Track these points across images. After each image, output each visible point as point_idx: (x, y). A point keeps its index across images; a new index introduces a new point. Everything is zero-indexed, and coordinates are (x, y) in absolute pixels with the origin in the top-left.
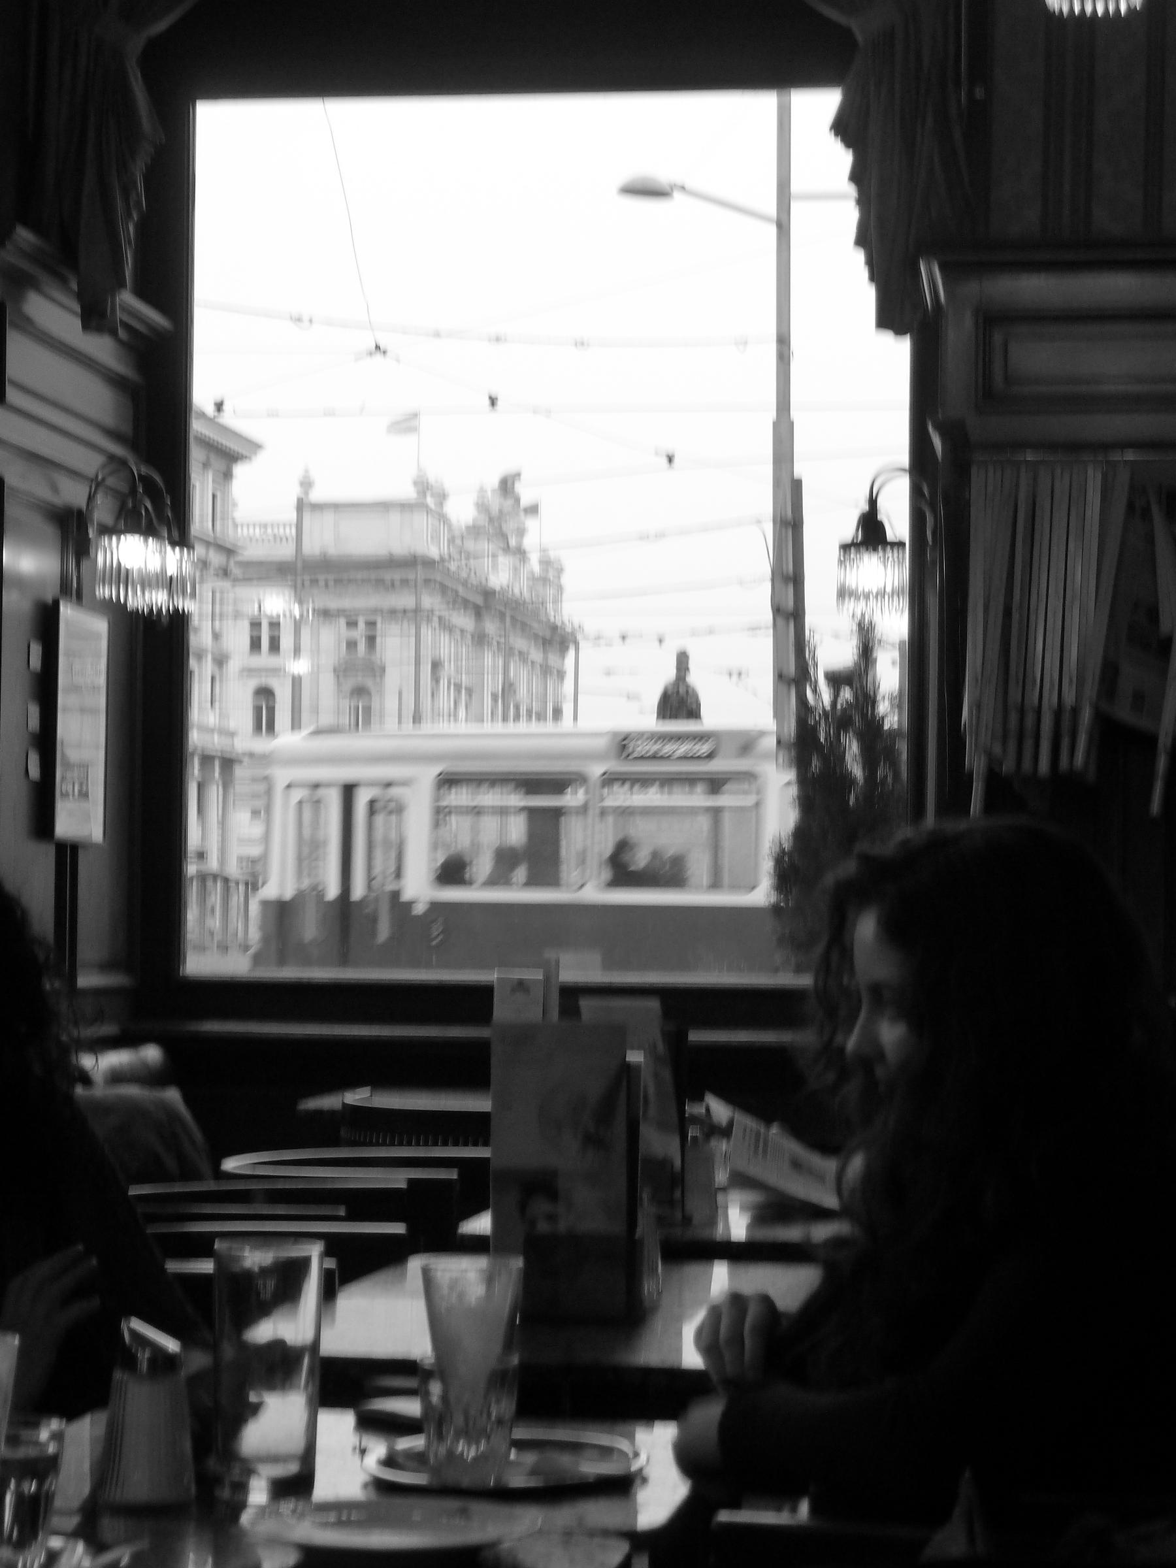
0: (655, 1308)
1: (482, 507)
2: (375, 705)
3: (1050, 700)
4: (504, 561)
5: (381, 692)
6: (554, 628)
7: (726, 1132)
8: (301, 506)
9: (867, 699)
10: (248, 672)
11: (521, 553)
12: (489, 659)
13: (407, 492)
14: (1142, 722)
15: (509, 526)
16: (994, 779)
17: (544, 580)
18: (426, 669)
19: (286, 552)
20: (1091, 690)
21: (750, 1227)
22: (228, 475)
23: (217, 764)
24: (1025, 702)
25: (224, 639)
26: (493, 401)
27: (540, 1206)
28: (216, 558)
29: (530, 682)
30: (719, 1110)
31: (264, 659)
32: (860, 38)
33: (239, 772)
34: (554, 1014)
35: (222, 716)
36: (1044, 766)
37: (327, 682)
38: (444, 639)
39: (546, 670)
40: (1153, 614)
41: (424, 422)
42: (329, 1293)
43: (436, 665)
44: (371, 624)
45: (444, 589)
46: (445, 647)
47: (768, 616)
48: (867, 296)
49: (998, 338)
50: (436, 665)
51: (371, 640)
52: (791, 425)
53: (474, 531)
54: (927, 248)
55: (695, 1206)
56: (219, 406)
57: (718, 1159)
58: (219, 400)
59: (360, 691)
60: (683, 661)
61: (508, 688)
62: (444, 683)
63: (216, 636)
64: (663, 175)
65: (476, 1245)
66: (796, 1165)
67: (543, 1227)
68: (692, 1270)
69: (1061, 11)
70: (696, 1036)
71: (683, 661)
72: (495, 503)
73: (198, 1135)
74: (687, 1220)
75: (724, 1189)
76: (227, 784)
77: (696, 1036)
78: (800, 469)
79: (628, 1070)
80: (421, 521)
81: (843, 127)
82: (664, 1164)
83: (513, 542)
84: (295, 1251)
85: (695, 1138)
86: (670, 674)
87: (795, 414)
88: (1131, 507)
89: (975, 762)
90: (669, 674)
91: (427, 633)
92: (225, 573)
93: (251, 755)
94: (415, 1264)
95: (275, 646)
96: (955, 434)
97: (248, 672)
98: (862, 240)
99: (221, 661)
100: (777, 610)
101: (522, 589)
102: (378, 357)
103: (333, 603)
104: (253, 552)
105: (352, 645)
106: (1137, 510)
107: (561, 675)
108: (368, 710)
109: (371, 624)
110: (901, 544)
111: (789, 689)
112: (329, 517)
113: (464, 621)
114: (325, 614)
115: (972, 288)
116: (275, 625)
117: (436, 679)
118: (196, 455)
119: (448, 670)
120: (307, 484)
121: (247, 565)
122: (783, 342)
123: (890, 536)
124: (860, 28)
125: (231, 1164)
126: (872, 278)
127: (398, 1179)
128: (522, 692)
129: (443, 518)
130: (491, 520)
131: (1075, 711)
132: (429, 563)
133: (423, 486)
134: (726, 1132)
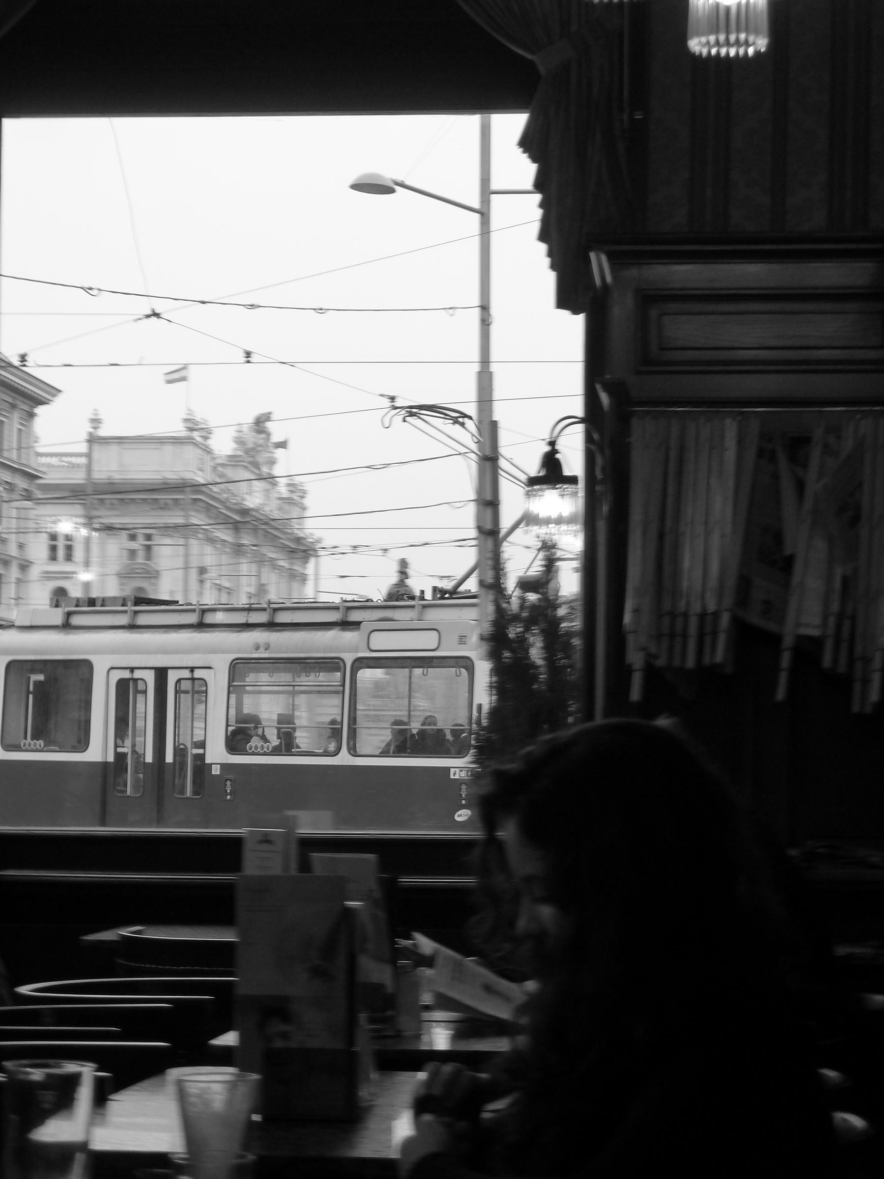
0: (368, 1109)
1: (240, 441)
3: (696, 608)
4: (258, 485)
6: (298, 540)
7: (429, 961)
8: (93, 440)
9: (549, 604)
10: (48, 576)
11: (271, 479)
12: (246, 567)
13: (178, 429)
14: (771, 626)
15: (262, 458)
16: (651, 673)
17: (289, 501)
18: (193, 575)
19: (78, 477)
20: (728, 601)
24: (486, 1113)
26: (248, 354)
27: (277, 1027)
30: (425, 944)
31: (61, 566)
32: (542, 70)
36: (691, 663)
38: (209, 549)
40: (778, 538)
41: (192, 373)
42: (101, 1098)
43: (202, 570)
45: (208, 508)
46: (209, 556)
47: (473, 533)
48: (548, 280)
49: (654, 313)
50: (202, 570)
51: (148, 548)
53: (233, 461)
54: (597, 242)
55: (405, 1022)
56: (23, 358)
58: (22, 352)
60: (404, 564)
62: (208, 584)
63: (21, 546)
64: (388, 173)
65: (223, 1057)
66: (488, 989)
67: (279, 1044)
69: (701, 53)
70: (406, 880)
72: (251, 438)
74: (398, 1036)
75: (427, 1008)
77: (406, 880)
78: (499, 413)
79: (349, 913)
80: (190, 453)
81: (527, 143)
82: (379, 987)
83: (265, 469)
84: (71, 1067)
86: (394, 579)
87: (494, 367)
88: (761, 453)
89: (635, 658)
90: (393, 578)
92: (28, 496)
94: (174, 1073)
95: (69, 557)
96: (617, 390)
97: (48, 576)
98: (543, 236)
101: (272, 509)
102: (154, 319)
103: (116, 521)
104: (51, 478)
105: (132, 553)
106: (765, 454)
107: (303, 579)
109: (149, 537)
110: (573, 480)
112: (114, 449)
113: (225, 535)
114: (109, 529)
115: (632, 272)
116: (68, 538)
119: (212, 574)
120: (96, 422)
122: (485, 308)
123: (567, 472)
124: (543, 62)
125: (24, 990)
126: (553, 267)
127: (161, 1002)
129: (208, 451)
130: (247, 451)
131: (716, 615)
132: (196, 487)
133: (192, 424)
134: (429, 961)
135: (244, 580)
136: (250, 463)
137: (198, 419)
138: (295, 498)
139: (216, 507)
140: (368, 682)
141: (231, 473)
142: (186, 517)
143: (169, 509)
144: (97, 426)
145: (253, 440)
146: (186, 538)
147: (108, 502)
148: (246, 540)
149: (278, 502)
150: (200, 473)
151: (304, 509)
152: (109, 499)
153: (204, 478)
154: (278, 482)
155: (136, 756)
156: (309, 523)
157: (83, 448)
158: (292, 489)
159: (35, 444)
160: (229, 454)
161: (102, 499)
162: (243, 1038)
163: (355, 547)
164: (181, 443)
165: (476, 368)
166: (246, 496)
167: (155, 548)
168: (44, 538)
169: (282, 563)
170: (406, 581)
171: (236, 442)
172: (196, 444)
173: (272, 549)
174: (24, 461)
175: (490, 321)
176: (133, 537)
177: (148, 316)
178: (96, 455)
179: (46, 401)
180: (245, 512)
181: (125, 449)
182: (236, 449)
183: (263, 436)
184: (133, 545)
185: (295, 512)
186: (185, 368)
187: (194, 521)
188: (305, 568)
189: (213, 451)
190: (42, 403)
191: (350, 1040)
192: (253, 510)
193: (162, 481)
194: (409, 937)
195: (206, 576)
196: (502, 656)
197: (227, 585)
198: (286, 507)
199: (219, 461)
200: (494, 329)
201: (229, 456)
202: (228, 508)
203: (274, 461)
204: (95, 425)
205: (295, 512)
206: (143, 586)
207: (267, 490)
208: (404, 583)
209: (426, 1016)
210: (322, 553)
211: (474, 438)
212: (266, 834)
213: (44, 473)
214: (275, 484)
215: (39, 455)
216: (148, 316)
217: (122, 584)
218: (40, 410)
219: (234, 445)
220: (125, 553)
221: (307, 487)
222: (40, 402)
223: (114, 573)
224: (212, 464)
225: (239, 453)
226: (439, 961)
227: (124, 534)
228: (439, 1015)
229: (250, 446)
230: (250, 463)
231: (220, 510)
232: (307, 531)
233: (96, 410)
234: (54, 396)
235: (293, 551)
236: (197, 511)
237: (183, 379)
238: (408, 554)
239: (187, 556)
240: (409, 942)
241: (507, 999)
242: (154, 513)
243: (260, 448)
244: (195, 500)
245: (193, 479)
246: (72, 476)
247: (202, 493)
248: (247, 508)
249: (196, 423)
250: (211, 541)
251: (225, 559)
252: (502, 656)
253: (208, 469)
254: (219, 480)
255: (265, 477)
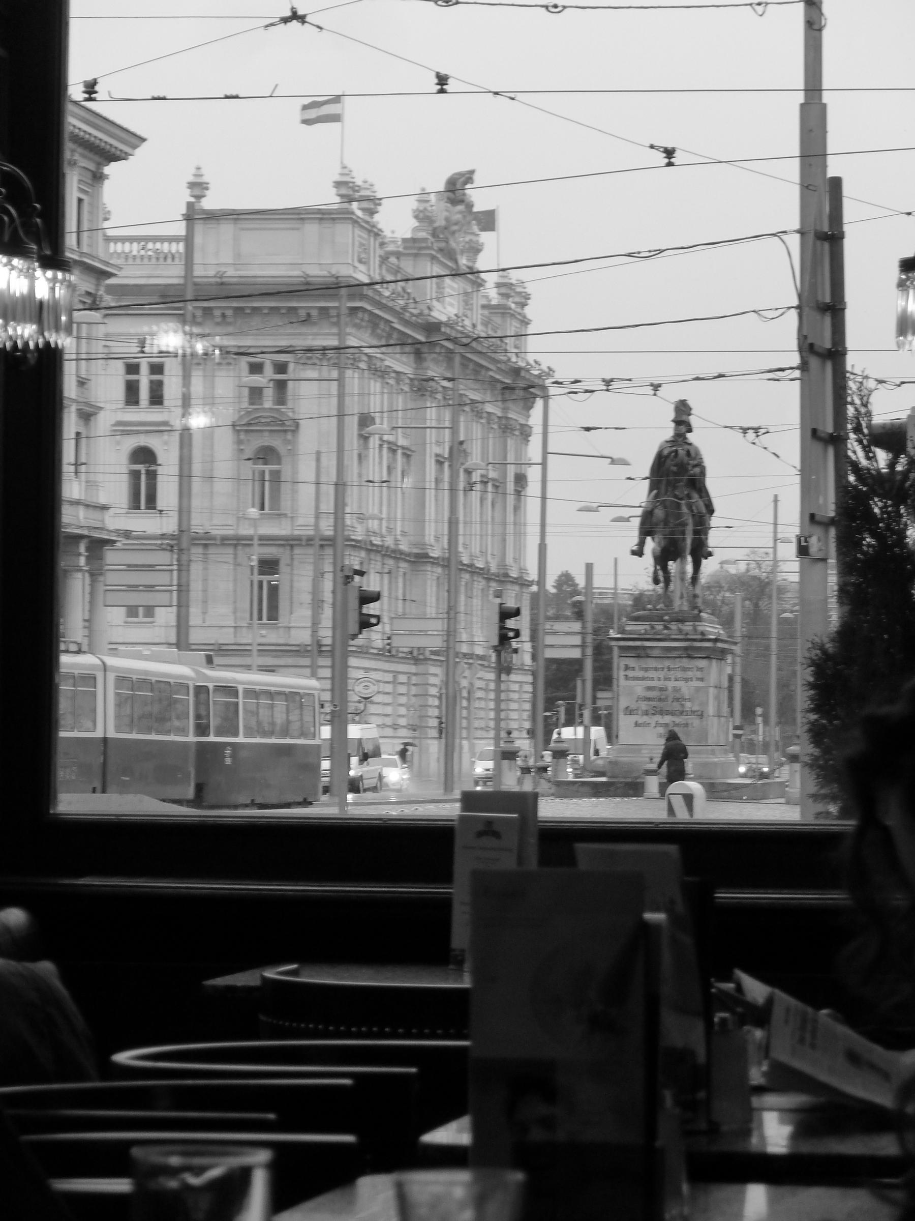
1: (423, 216)
2: (286, 475)
5: (293, 453)
8: (192, 216)
10: (123, 429)
11: (472, 275)
13: (329, 198)
15: (458, 242)
17: (502, 311)
18: (352, 424)
19: (172, 274)
21: (795, 1137)
22: (98, 178)
23: (82, 548)
25: (92, 385)
26: (442, 80)
28: (85, 284)
29: (484, 439)
31: (144, 414)
33: (111, 557)
34: (532, 863)
35: (91, 485)
37: (225, 443)
38: (375, 386)
39: (506, 428)
43: (365, 420)
44: (281, 368)
45: (374, 322)
50: (365, 420)
51: (281, 386)
52: (824, 107)
53: (413, 247)
57: (752, 1050)
58: (89, 78)
59: (266, 455)
60: (683, 410)
61: (458, 449)
62: (374, 442)
63: (82, 383)
66: (854, 1058)
68: (722, 1193)
70: (723, 895)
71: (683, 410)
72: (441, 211)
73: (79, 1021)
74: (714, 1130)
75: (760, 1090)
76: (95, 574)
77: (723, 895)
78: (592, 431)
80: (345, 234)
83: (463, 261)
85: (723, 1021)
86: (669, 432)
91: (353, 379)
93: (127, 534)
95: (157, 399)
97: (123, 429)
99: (87, 416)
100: (807, 348)
105: (256, 393)
107: (525, 433)
108: (276, 478)
109: (281, 368)
111: (825, 451)
112: (227, 229)
117: (365, 438)
118: (70, 151)
119: (382, 425)
120: (198, 187)
121: (121, 290)
125: (123, 1057)
128: (475, 458)
129: (374, 232)
135: (431, 436)
136: (441, 250)
137: (359, 182)
138: (513, 306)
139: (387, 321)
140: (220, 703)
141: (409, 267)
142: (341, 335)
143: (315, 324)
144: (203, 194)
145: (446, 214)
146: (341, 368)
147: (217, 313)
148: (434, 370)
149: (486, 312)
150: (362, 267)
151: (525, 322)
152: (220, 308)
153: (369, 276)
154: (485, 282)
155: (303, 700)
156: (532, 344)
157: (180, 229)
158: (503, 290)
159: (106, 224)
160: (408, 235)
161: (210, 309)
162: (477, 1130)
163: (608, 382)
164: (333, 219)
165: (800, 98)
166: (435, 303)
167: (290, 384)
168: (119, 367)
169: (489, 408)
170: (689, 435)
171: (416, 217)
172: (355, 222)
173: (477, 386)
174: (85, 249)
175: (823, 23)
176: (256, 368)
177: (285, 20)
178: (198, 240)
179: (123, 155)
180: (432, 328)
181: (243, 229)
182: (415, 230)
183: (461, 207)
184: (257, 380)
185: (512, 328)
186: (337, 99)
187: (352, 342)
188: (528, 416)
189: (382, 232)
190: (116, 159)
191: (651, 1132)
192: (446, 324)
193: (303, 280)
194: (728, 978)
195: (371, 429)
196: (864, 542)
197: (402, 442)
198: (497, 320)
199: (391, 248)
200: (828, 37)
201: (405, 240)
202: (407, 323)
203: (480, 247)
204: (197, 192)
205: (512, 328)
206: (274, 445)
207: (466, 294)
208: (686, 438)
209: (756, 1101)
210: (553, 390)
211: (469, 276)
212: (489, 822)
213: (120, 268)
214: (479, 284)
215: (108, 239)
216: (285, 20)
217: (239, 442)
218: (111, 169)
219: (414, 223)
220: (246, 392)
221: (530, 289)
222: (112, 157)
223: (230, 424)
224: (380, 252)
225: (422, 235)
226: (778, 1014)
227: (244, 361)
228: (771, 1099)
229: (440, 222)
230: (441, 250)
231: (393, 325)
232: (531, 358)
233: (198, 168)
234: (135, 147)
235: (507, 388)
236: (358, 327)
237: (335, 118)
238: (693, 394)
239: (341, 396)
240: (730, 986)
241: (886, 1076)
242: (289, 330)
243: (455, 228)
244: (354, 310)
245: (351, 277)
246: (165, 273)
247: (363, 297)
248: (436, 321)
249: (355, 188)
250: (381, 373)
251: (399, 402)
252: (864, 542)
253: (375, 262)
254: (389, 278)
255: (464, 272)
